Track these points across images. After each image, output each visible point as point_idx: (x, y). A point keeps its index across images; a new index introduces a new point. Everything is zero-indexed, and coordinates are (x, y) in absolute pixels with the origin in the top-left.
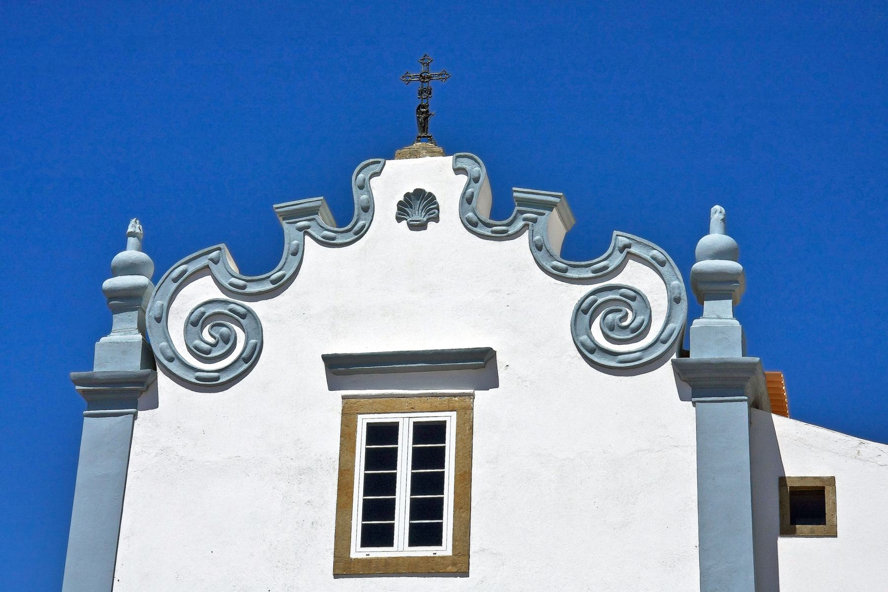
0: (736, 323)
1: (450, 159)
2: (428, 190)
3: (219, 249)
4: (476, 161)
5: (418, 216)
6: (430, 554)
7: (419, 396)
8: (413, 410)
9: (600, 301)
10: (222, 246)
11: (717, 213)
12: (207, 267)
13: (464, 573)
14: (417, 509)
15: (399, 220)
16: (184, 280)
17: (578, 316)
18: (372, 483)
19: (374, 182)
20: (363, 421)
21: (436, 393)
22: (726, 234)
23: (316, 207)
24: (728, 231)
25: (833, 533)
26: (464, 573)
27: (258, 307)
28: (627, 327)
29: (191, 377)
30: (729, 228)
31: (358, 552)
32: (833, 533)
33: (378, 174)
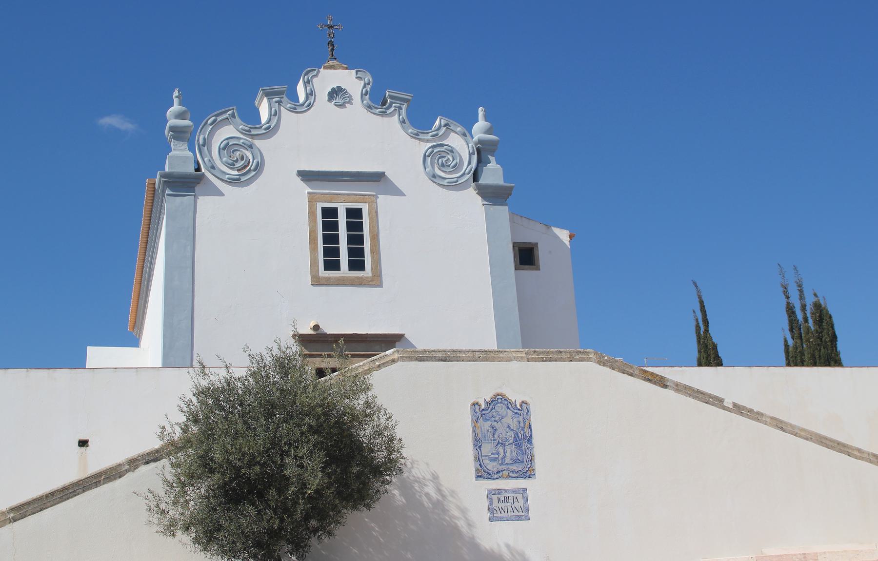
0: (499, 166)
1: (354, 72)
2: (335, 87)
3: (233, 109)
4: (364, 72)
5: (339, 100)
6: (361, 276)
7: (348, 195)
8: (345, 202)
9: (435, 151)
10: (235, 107)
11: (481, 112)
12: (228, 118)
13: (380, 285)
14: (352, 252)
15: (330, 100)
16: (216, 125)
17: (221, 152)
18: (360, 240)
19: (315, 80)
20: (320, 206)
21: (342, 193)
22: (486, 121)
23: (282, 91)
24: (180, 104)
25: (538, 269)
26: (380, 285)
27: (257, 143)
28: (449, 166)
29: (445, 182)
30: (486, 118)
31: (323, 273)
32: (538, 269)
33: (316, 76)
